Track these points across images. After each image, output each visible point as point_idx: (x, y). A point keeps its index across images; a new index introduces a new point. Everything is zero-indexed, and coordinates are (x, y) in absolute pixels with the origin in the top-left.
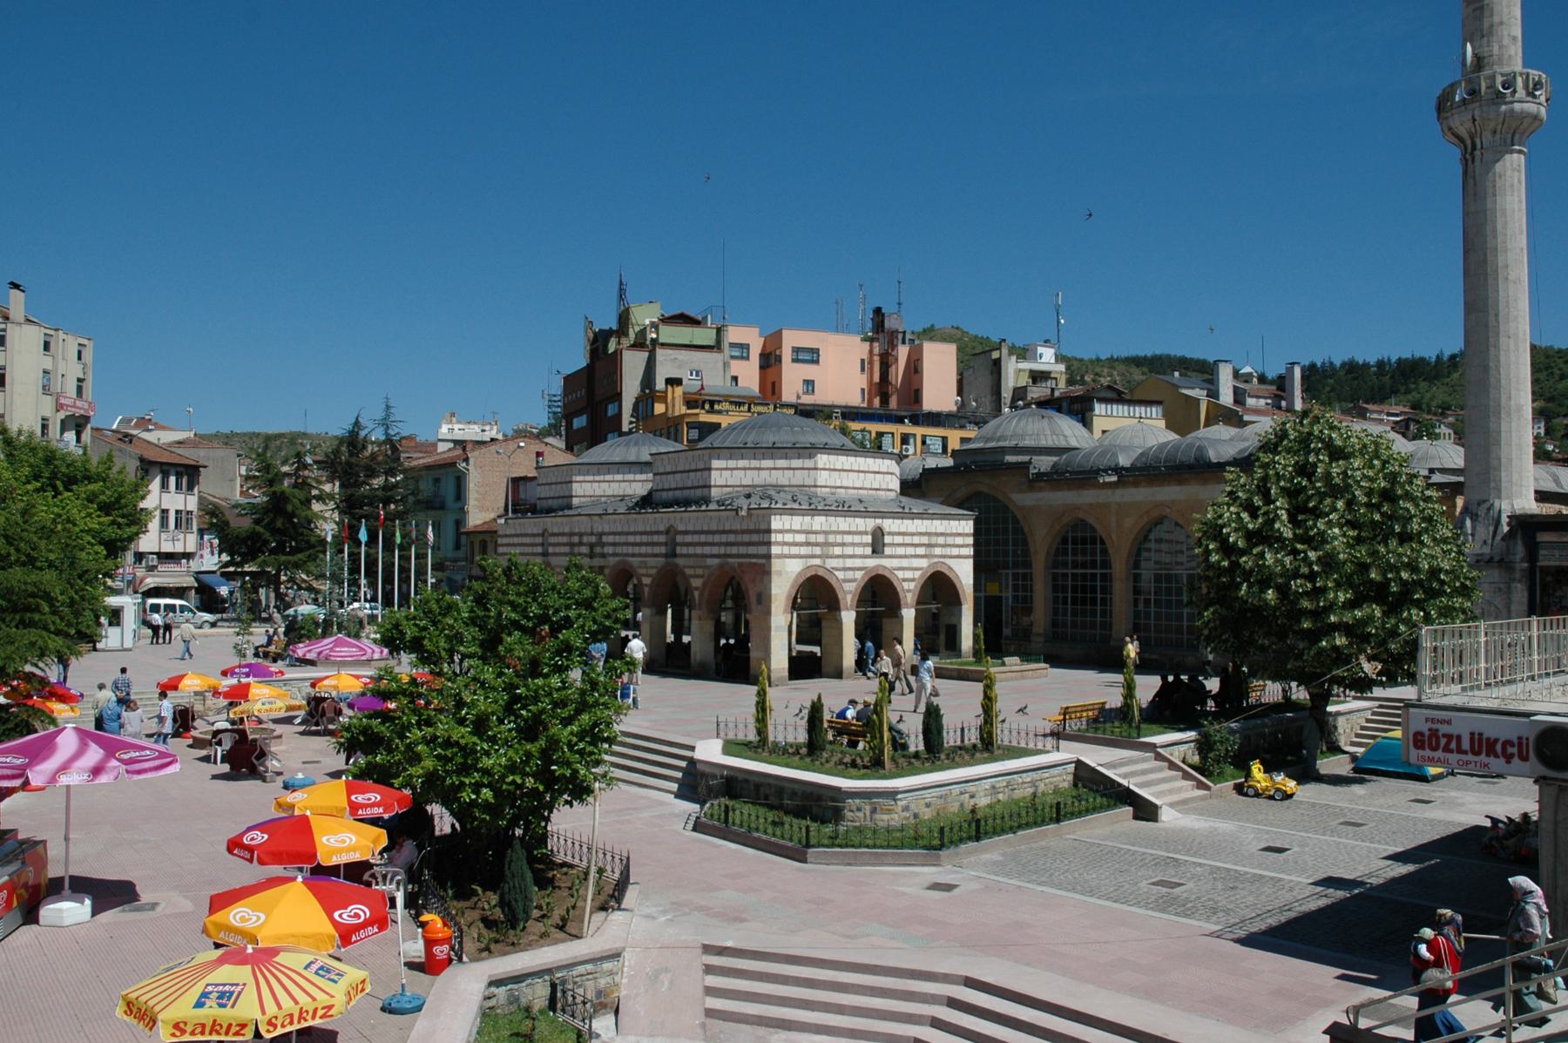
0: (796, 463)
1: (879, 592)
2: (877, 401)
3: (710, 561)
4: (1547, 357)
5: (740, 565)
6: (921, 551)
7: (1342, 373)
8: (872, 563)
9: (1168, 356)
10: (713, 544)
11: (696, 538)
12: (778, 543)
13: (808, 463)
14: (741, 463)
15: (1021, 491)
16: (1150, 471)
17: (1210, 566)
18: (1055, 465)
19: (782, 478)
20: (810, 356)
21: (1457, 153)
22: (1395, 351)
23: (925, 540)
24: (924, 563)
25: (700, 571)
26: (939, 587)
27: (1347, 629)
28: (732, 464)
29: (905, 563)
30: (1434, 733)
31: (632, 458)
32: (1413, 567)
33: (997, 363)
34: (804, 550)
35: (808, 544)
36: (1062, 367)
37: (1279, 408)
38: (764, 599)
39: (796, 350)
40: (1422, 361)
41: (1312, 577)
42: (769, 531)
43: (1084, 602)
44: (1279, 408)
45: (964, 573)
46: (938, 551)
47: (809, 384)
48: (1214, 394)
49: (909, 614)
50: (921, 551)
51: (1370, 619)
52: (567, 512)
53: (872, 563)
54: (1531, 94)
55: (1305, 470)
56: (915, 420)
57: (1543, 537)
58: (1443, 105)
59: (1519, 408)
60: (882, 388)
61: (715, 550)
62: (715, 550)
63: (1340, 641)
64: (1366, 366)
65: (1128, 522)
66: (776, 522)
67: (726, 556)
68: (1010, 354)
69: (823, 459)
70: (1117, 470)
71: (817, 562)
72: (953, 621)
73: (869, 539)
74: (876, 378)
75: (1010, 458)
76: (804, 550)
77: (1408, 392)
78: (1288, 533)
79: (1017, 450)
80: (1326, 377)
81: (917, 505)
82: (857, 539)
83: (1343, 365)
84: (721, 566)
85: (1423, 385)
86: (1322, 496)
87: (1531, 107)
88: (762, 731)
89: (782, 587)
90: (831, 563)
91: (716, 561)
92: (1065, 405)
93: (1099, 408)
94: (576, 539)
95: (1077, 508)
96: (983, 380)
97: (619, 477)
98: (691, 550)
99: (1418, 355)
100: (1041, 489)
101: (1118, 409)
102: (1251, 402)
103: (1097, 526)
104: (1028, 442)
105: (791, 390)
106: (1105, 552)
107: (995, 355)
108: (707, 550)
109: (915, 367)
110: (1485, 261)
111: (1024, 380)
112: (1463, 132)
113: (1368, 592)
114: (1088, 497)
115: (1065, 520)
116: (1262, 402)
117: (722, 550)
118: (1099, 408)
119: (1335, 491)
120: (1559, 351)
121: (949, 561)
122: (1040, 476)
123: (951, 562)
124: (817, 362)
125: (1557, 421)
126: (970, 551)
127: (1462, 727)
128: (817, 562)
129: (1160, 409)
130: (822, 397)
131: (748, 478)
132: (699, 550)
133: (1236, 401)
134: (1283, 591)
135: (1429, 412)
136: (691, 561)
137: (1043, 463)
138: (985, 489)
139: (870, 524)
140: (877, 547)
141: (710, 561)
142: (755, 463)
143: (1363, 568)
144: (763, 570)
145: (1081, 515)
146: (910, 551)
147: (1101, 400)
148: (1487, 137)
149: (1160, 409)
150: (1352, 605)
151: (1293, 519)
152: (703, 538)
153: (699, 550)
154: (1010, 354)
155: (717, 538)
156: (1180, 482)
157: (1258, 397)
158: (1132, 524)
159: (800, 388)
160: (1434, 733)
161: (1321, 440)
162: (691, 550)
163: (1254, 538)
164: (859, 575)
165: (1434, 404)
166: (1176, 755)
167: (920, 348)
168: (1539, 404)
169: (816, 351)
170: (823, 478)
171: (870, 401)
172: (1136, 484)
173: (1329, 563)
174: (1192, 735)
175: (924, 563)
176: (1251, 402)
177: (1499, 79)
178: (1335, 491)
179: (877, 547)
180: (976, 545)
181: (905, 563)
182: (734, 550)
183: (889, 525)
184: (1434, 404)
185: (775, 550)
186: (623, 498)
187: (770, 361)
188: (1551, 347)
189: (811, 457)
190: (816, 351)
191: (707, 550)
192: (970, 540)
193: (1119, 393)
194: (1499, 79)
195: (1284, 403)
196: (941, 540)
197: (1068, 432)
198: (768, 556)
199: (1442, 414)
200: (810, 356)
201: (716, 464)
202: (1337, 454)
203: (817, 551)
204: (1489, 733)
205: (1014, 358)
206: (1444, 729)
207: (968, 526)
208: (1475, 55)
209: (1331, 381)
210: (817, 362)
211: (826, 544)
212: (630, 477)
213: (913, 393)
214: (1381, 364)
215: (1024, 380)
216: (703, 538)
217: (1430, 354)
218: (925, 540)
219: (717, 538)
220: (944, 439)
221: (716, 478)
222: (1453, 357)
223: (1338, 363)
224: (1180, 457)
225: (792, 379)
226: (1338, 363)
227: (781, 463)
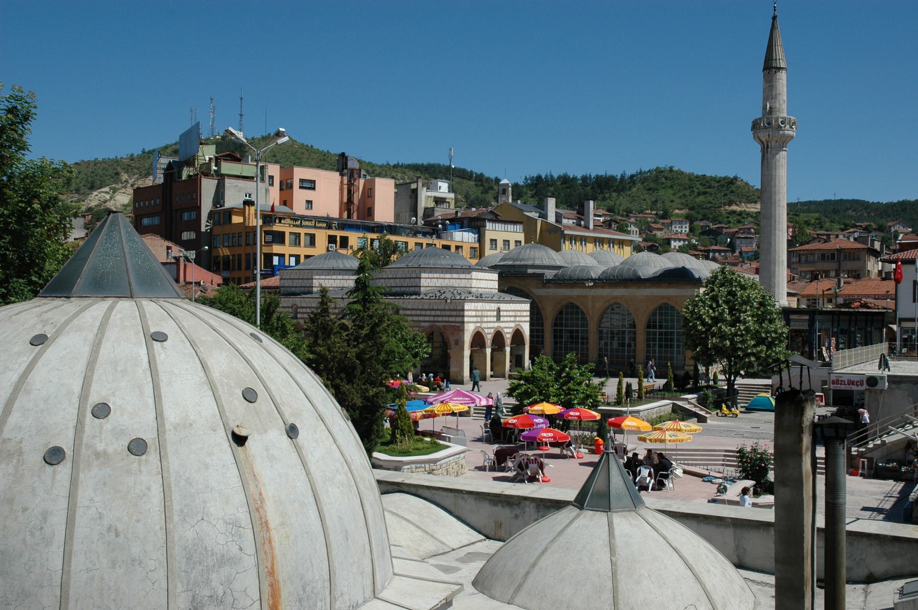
0: (462, 276)
1: (498, 337)
2: (345, 214)
3: (423, 324)
4: (690, 180)
5: (444, 326)
6: (512, 319)
7: (559, 183)
8: (496, 325)
9: (439, 165)
10: (426, 316)
12: (469, 316)
13: (468, 276)
14: (436, 275)
15: (538, 288)
16: (610, 280)
17: (698, 331)
18: (555, 276)
19: (456, 283)
20: (309, 185)
21: (759, 147)
22: (596, 169)
23: (513, 313)
24: (513, 325)
26: (517, 335)
27: (753, 354)
28: (431, 275)
29: (507, 325)
31: (341, 267)
32: (775, 332)
33: (415, 192)
34: (475, 319)
35: (476, 316)
36: (452, 195)
37: (580, 225)
38: (460, 343)
39: (302, 181)
40: (612, 179)
41: (742, 335)
42: (463, 310)
43: (666, 346)
44: (580, 225)
45: (526, 329)
46: (518, 319)
47: (309, 202)
48: (544, 216)
49: (508, 349)
50: (512, 319)
51: (761, 351)
52: (309, 296)
53: (496, 325)
54: (791, 127)
55: (732, 293)
56: (371, 229)
57: (792, 317)
58: (755, 126)
59: (783, 262)
60: (347, 205)
61: (427, 319)
62: (427, 319)
63: (753, 359)
64: (575, 179)
65: (598, 305)
66: (467, 306)
67: (434, 321)
68: (423, 186)
69: (475, 274)
70: (592, 280)
71: (479, 325)
72: (520, 353)
73: (495, 313)
74: (345, 200)
75: (530, 271)
76: (475, 319)
77: (604, 199)
78: (729, 318)
79: (533, 267)
80: (549, 186)
81: (508, 297)
82: (489, 313)
83: (559, 177)
84: (431, 327)
85: (614, 194)
86: (741, 305)
87: (791, 133)
88: (801, 369)
89: (468, 338)
90: (484, 325)
91: (428, 324)
92: (466, 222)
93: (489, 225)
95: (570, 297)
96: (406, 202)
97: (340, 277)
99: (609, 173)
100: (549, 287)
101: (499, 226)
102: (565, 221)
103: (581, 307)
104: (537, 263)
105: (299, 208)
106: (584, 319)
107: (413, 186)
108: (421, 318)
109: (369, 193)
110: (771, 197)
111: (431, 204)
112: (763, 139)
113: (760, 341)
114: (575, 292)
115: (564, 302)
116: (571, 221)
117: (432, 319)
118: (489, 225)
119: (747, 302)
120: (697, 177)
121: (521, 324)
122: (549, 281)
123: (521, 324)
124: (314, 189)
125: (696, 223)
126: (528, 319)
127: (845, 378)
128: (479, 325)
129: (521, 226)
130: (319, 210)
131: (439, 283)
133: (557, 221)
134: (732, 341)
135: (618, 214)
137: (549, 274)
138: (516, 286)
139: (494, 306)
140: (498, 317)
141: (423, 324)
142: (442, 276)
143: (757, 332)
144: (459, 328)
145: (572, 301)
147: (490, 220)
148: (773, 143)
149: (521, 226)
150: (754, 346)
151: (730, 313)
152: (418, 312)
154: (423, 186)
155: (428, 313)
156: (626, 287)
157: (569, 219)
158: (599, 305)
159: (304, 204)
161: (736, 281)
163: (716, 320)
164: (492, 331)
165: (621, 208)
166: (693, 401)
167: (372, 183)
169: (314, 182)
170: (475, 284)
171: (341, 214)
172: (603, 287)
173: (747, 330)
174: (695, 396)
175: (513, 325)
176: (565, 221)
177: (780, 120)
178: (745, 303)
179: (498, 317)
180: (531, 316)
181: (507, 325)
182: (440, 319)
183: (503, 306)
184: (621, 208)
185: (466, 319)
186: (342, 288)
187: (286, 187)
188: (693, 174)
189: (469, 273)
190: (314, 182)
191: (421, 318)
192: (528, 313)
193: (496, 215)
194: (780, 120)
195: (583, 223)
196: (518, 314)
197: (555, 258)
198: (463, 322)
199: (627, 216)
200: (309, 185)
201: (423, 275)
202: (743, 288)
203: (479, 319)
204: (853, 379)
205: (425, 189)
207: (527, 307)
208: (770, 108)
209: (552, 189)
210: (314, 189)
211: (482, 316)
212: (347, 277)
213: (369, 212)
214: (584, 179)
215: (431, 204)
216: (418, 312)
217: (617, 173)
218: (513, 313)
219: (428, 313)
220: (406, 243)
221: (424, 282)
222: (632, 176)
223: (556, 176)
224: (626, 276)
225: (300, 196)
226: (556, 176)
227: (455, 276)
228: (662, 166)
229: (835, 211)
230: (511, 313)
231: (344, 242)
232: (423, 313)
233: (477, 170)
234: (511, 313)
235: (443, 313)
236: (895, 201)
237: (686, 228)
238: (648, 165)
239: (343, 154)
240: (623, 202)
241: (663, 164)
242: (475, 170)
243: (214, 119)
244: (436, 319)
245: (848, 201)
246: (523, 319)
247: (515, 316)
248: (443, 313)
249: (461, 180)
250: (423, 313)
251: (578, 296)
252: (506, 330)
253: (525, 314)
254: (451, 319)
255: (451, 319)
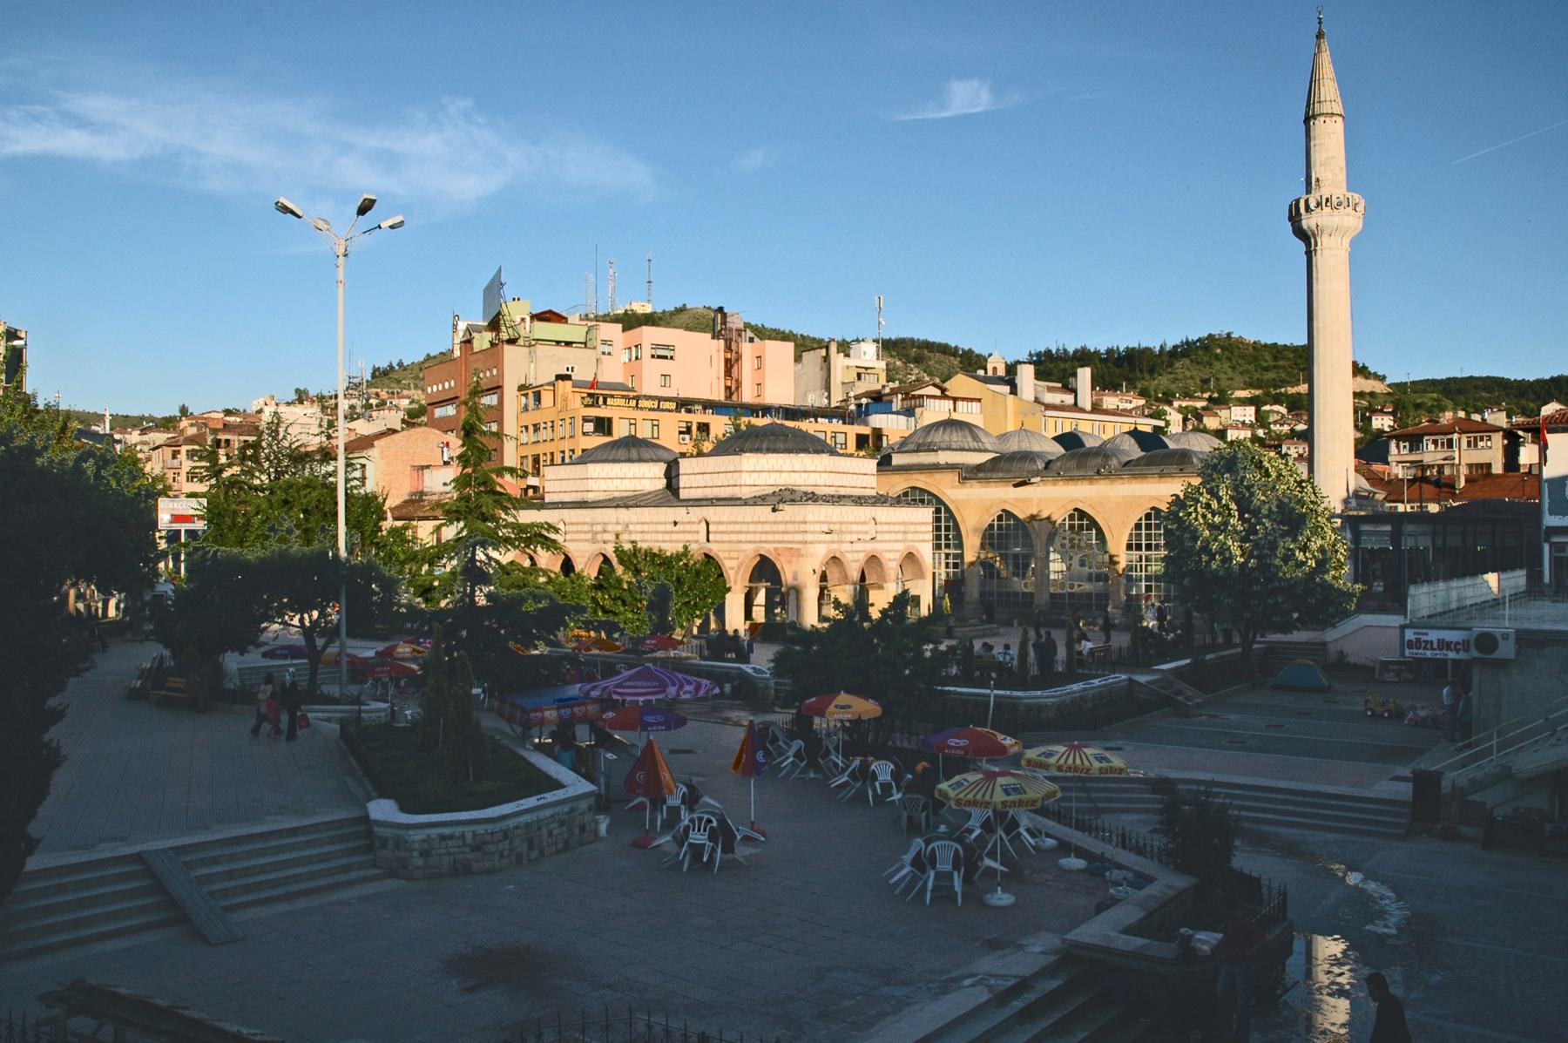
3: (744, 546)
6: (900, 537)
11: (731, 528)
23: (902, 528)
24: (901, 546)
25: (735, 555)
29: (889, 546)
30: (1418, 640)
50: (900, 537)
57: (1365, 528)
62: (750, 537)
64: (1097, 353)
71: (835, 546)
83: (1076, 351)
91: (752, 546)
94: (599, 528)
98: (726, 537)
99: (1143, 345)
108: (742, 537)
117: (757, 538)
120: (1266, 345)
121: (918, 545)
123: (918, 545)
128: (835, 546)
132: (734, 537)
136: (726, 546)
146: (893, 537)
153: (734, 537)
155: (752, 528)
159: (659, 380)
160: (1418, 640)
162: (726, 537)
168: (1359, 435)
181: (889, 546)
182: (770, 537)
191: (742, 537)
196: (912, 528)
206: (1424, 638)
214: (1110, 351)
216: (737, 528)
217: (1155, 345)
219: (752, 528)
223: (1071, 350)
226: (1071, 350)
228: (1215, 332)
229: (1460, 391)
230: (897, 528)
231: (704, 428)
232: (745, 528)
233: (964, 345)
234: (897, 528)
235: (775, 528)
236: (1547, 377)
237: (1249, 414)
238: (1196, 332)
239: (721, 309)
240: (1162, 382)
241: (1218, 330)
242: (961, 346)
243: (614, 289)
244: (764, 537)
245: (1480, 378)
246: (921, 537)
247: (905, 533)
248: (775, 528)
249: (943, 357)
250: (745, 528)
251: (1016, 500)
252: (887, 556)
253: (924, 528)
254: (787, 537)
255: (787, 537)
